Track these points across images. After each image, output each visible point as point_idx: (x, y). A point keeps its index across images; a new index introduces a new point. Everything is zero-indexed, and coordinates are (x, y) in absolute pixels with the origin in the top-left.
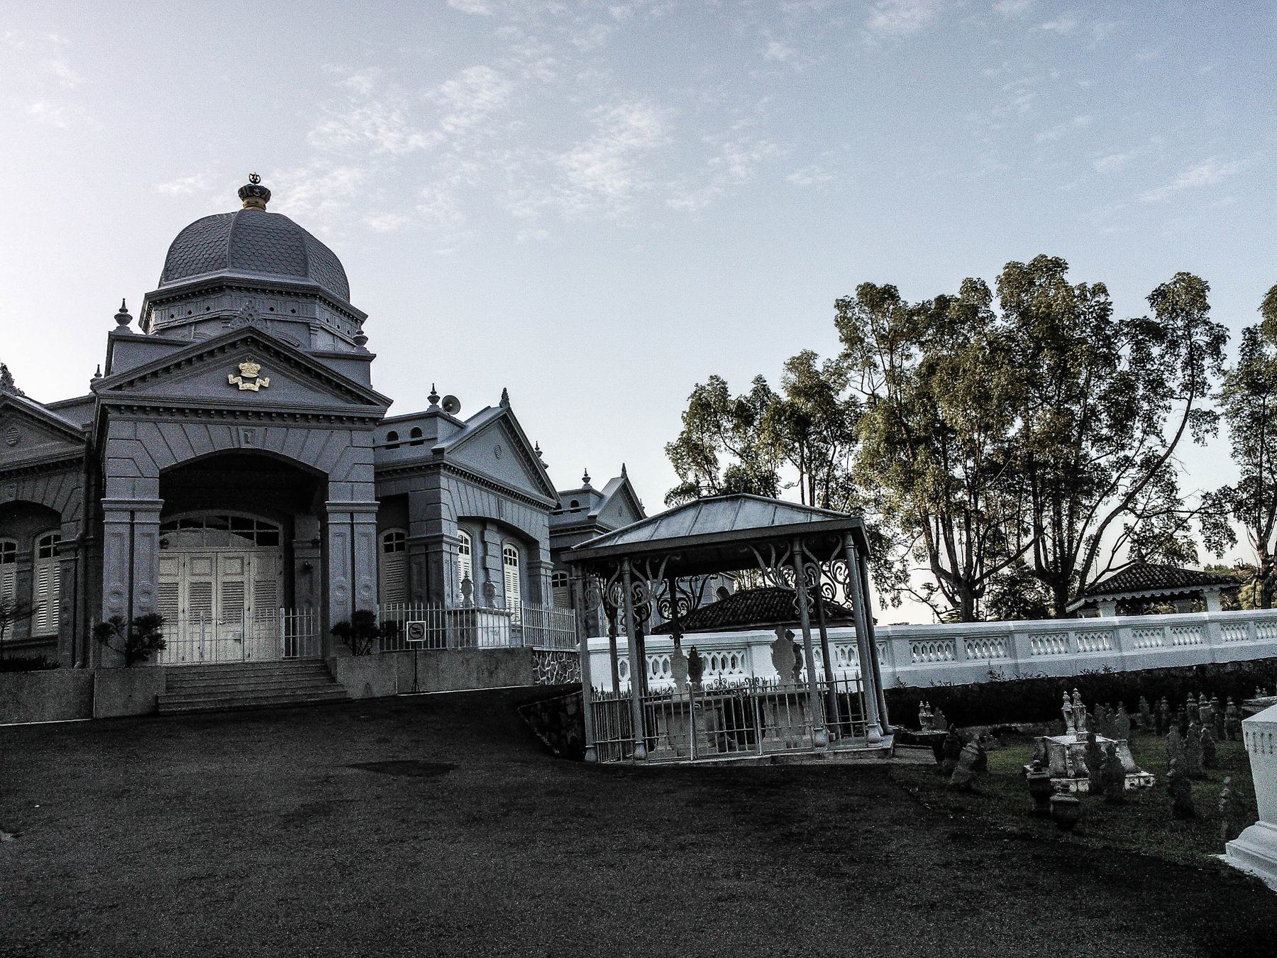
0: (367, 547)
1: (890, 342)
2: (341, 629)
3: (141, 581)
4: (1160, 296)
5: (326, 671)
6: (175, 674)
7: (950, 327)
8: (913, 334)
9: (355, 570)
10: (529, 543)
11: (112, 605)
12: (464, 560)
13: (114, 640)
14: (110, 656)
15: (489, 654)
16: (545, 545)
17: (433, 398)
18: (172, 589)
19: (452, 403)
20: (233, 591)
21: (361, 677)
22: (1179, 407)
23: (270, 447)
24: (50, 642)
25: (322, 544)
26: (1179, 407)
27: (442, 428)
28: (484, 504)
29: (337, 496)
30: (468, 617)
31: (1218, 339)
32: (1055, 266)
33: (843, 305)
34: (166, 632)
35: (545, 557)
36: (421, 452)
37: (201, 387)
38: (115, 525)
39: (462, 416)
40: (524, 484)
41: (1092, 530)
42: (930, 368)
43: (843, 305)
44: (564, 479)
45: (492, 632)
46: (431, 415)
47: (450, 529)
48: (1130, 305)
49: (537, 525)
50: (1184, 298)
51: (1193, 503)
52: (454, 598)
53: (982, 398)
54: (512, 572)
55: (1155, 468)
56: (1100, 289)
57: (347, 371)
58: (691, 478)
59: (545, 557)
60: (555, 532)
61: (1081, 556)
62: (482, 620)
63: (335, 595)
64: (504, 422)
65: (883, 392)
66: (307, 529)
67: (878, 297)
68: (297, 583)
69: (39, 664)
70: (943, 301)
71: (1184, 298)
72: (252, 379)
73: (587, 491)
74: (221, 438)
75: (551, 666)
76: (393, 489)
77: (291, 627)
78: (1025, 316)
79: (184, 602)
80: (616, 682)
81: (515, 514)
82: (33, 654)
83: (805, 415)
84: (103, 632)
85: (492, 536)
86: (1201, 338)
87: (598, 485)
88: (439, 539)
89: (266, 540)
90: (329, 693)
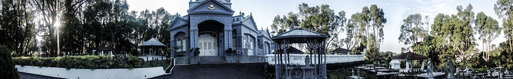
0: (231, 36)
1: (306, 12)
2: (227, 51)
3: (196, 42)
4: (340, 13)
5: (224, 58)
6: (202, 58)
7: (314, 12)
8: (309, 12)
9: (229, 42)
10: (254, 38)
11: (192, 46)
12: (245, 40)
13: (193, 52)
14: (192, 54)
15: (251, 56)
16: (256, 39)
17: (240, 13)
18: (201, 44)
19: (243, 14)
20: (210, 44)
21: (231, 60)
22: (340, 28)
23: (218, 20)
24: (185, 52)
25: (223, 37)
26: (340, 28)
27: (242, 18)
28: (248, 31)
29: (226, 28)
30: (246, 50)
31: (346, 20)
32: (328, 6)
33: (300, 5)
34: (200, 50)
35: (256, 41)
36: (239, 22)
37: (204, 9)
38: (192, 33)
39: (245, 16)
40: (253, 28)
41: (328, 42)
42: (311, 17)
43: (300, 5)
44: (259, 29)
45: (250, 53)
46: (240, 16)
47: (243, 35)
48: (336, 14)
49: (255, 35)
50: (342, 14)
51: (340, 40)
52: (244, 47)
53: (318, 22)
54: (252, 43)
55: (336, 35)
56: (333, 11)
57: (227, 6)
58: (274, 30)
59: (256, 41)
60: (258, 37)
61: (326, 45)
62: (249, 50)
63: (226, 45)
64: (251, 18)
65: (304, 20)
66: (221, 34)
67: (305, 5)
68: (219, 43)
69: (182, 56)
70: (314, 8)
71: (342, 14)
72: (212, 7)
73: (262, 30)
74: (207, 18)
75: (260, 59)
76: (235, 28)
77: (218, 50)
78: (323, 12)
79: (203, 45)
80: (276, 63)
81: (252, 34)
82: (181, 54)
83: (293, 21)
84: (191, 51)
85: (249, 37)
86: (344, 19)
87: (264, 29)
88: (241, 37)
89: (215, 36)
90: (225, 62)
